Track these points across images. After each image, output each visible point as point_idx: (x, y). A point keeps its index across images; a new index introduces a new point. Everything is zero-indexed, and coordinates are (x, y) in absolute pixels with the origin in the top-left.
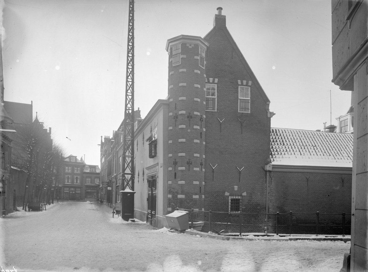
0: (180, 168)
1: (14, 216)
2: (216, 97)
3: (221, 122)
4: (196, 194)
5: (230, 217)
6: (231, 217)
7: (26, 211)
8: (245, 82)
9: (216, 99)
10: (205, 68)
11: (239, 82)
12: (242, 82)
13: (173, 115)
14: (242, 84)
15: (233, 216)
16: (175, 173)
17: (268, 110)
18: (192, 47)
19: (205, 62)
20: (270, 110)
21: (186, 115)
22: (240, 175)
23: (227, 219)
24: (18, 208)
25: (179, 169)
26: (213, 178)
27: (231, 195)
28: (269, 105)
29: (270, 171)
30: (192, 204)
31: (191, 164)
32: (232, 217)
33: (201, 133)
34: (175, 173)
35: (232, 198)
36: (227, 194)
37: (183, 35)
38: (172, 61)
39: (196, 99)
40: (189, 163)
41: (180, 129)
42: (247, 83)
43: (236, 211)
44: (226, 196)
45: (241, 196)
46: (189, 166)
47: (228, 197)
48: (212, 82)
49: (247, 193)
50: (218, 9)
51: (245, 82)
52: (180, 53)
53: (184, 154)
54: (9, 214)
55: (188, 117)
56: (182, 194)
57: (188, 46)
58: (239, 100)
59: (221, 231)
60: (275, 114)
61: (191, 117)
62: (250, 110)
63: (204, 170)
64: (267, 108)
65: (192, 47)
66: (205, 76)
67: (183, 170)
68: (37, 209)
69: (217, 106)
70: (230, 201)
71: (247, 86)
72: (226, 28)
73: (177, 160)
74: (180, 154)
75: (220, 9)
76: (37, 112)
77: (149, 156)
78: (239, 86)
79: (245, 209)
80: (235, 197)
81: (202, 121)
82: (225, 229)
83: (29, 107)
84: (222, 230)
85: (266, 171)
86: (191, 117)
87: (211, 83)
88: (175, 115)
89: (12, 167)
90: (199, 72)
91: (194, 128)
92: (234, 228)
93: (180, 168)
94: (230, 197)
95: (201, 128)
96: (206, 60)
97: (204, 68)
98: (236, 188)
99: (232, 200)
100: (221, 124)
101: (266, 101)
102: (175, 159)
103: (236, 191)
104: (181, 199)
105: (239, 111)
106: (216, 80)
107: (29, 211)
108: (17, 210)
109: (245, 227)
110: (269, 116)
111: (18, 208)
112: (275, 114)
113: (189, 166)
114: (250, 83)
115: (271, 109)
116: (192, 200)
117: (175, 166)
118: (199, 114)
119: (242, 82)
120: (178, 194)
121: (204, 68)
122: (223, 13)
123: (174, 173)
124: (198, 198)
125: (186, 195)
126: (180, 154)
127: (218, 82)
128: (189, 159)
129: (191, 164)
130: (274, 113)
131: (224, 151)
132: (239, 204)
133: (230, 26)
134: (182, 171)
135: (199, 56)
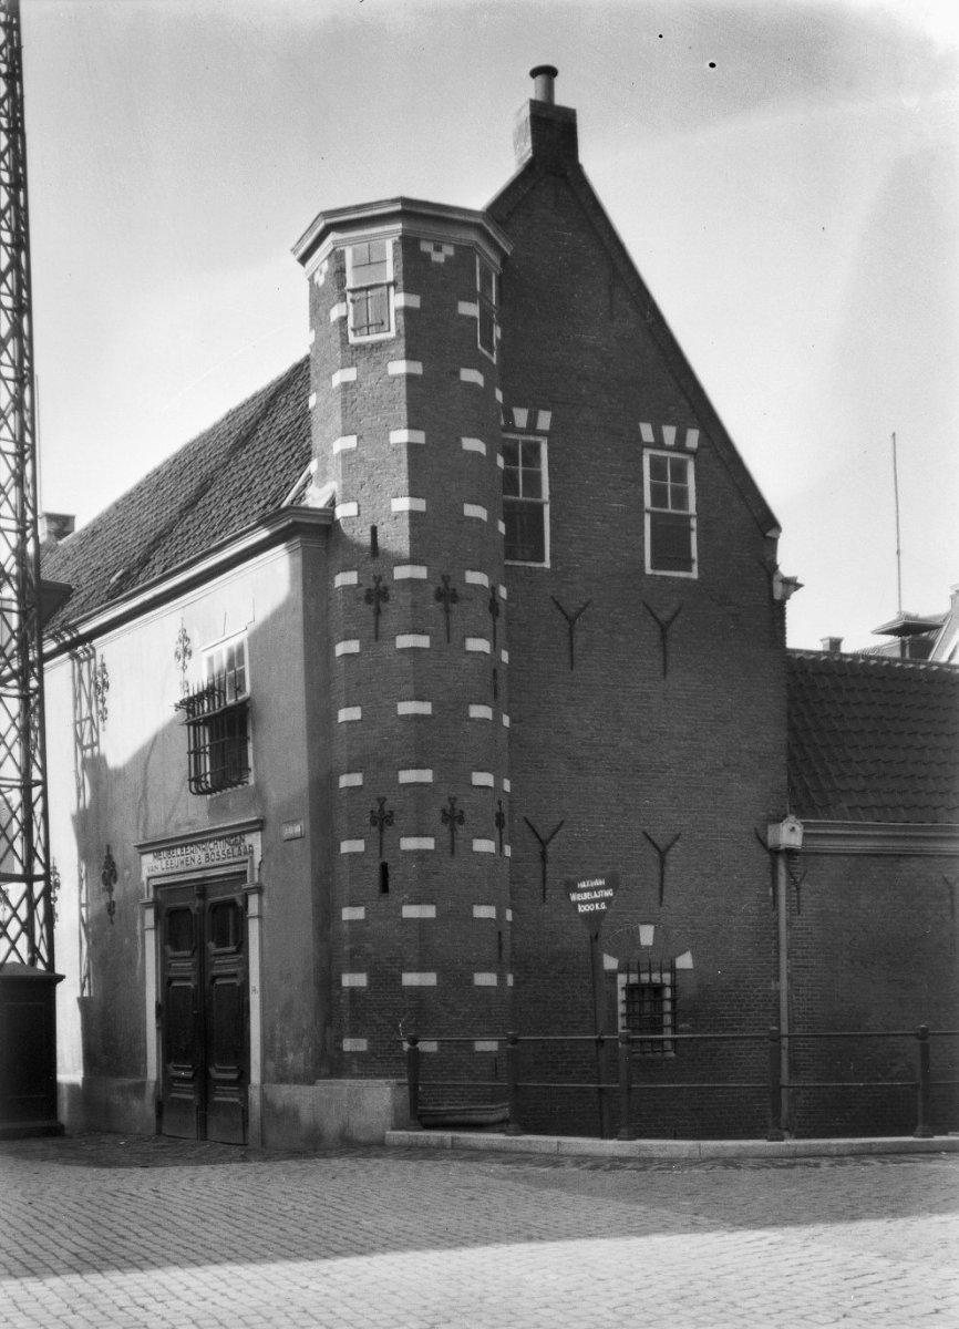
0: (409, 844)
2: (670, 510)
8: (669, 433)
11: (647, 432)
12: (658, 434)
13: (359, 585)
16: (384, 868)
17: (775, 567)
18: (447, 258)
19: (497, 332)
20: (781, 569)
21: (432, 588)
25: (402, 848)
27: (625, 968)
28: (774, 541)
29: (790, 853)
33: (495, 671)
34: (384, 868)
35: (634, 978)
36: (610, 963)
37: (405, 201)
38: (345, 318)
40: (453, 818)
41: (403, 651)
42: (681, 437)
45: (673, 970)
46: (453, 830)
47: (612, 975)
48: (547, 428)
49: (695, 958)
50: (535, 73)
51: (669, 433)
52: (389, 285)
53: (426, 776)
57: (429, 250)
60: (801, 586)
62: (695, 567)
63: (508, 851)
64: (768, 559)
65: (447, 258)
66: (499, 395)
67: (427, 851)
70: (621, 996)
71: (679, 451)
72: (578, 168)
73: (391, 804)
74: (407, 776)
75: (547, 73)
83: (792, 585)
85: (775, 852)
86: (454, 598)
88: (373, 585)
93: (409, 844)
94: (622, 979)
95: (494, 647)
96: (500, 323)
98: (647, 935)
99: (630, 989)
101: (765, 525)
105: (649, 571)
110: (778, 589)
112: (801, 586)
113: (453, 830)
114: (693, 438)
115: (789, 560)
117: (381, 830)
119: (658, 434)
122: (562, 98)
123: (378, 865)
124: (495, 983)
125: (442, 973)
126: (407, 776)
127: (701, 445)
128: (452, 800)
130: (798, 581)
131: (589, 759)
133: (598, 161)
134: (421, 855)
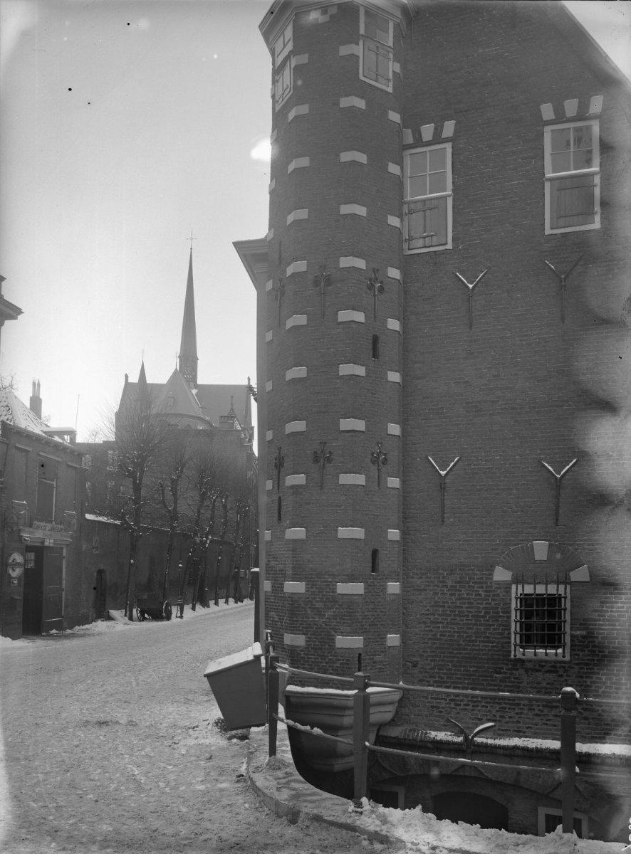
1: (92, 632)
3: (471, 286)
4: (351, 578)
5: (516, 673)
6: (521, 671)
7: (131, 619)
9: (450, 202)
10: (394, 89)
11: (547, 111)
14: (560, 117)
15: (529, 665)
22: (558, 497)
23: (502, 681)
24: (113, 613)
26: (443, 513)
27: (518, 580)
30: (335, 617)
31: (329, 460)
32: (527, 670)
36: (501, 575)
39: (345, 209)
43: (545, 648)
44: (498, 583)
47: (506, 587)
54: (77, 628)
55: (316, 283)
56: (295, 578)
58: (547, 185)
59: (477, 726)
61: (329, 281)
68: (159, 614)
69: (454, 227)
76: (232, 397)
77: (75, 435)
78: (548, 129)
79: (583, 637)
80: (532, 586)
81: (381, 290)
82: (493, 721)
84: (481, 721)
86: (329, 281)
87: (429, 144)
89: (88, 516)
90: (361, 104)
91: (340, 320)
92: (537, 720)
97: (390, 90)
100: (470, 295)
102: (280, 449)
103: (541, 562)
104: (293, 598)
105: (548, 231)
106: (449, 128)
107: (143, 619)
108: (110, 618)
109: (586, 718)
111: (113, 613)
116: (334, 600)
118: (361, 264)
120: (286, 578)
121: (390, 90)
127: (456, 131)
129: (329, 460)
132: (560, 618)
135: (357, 44)
